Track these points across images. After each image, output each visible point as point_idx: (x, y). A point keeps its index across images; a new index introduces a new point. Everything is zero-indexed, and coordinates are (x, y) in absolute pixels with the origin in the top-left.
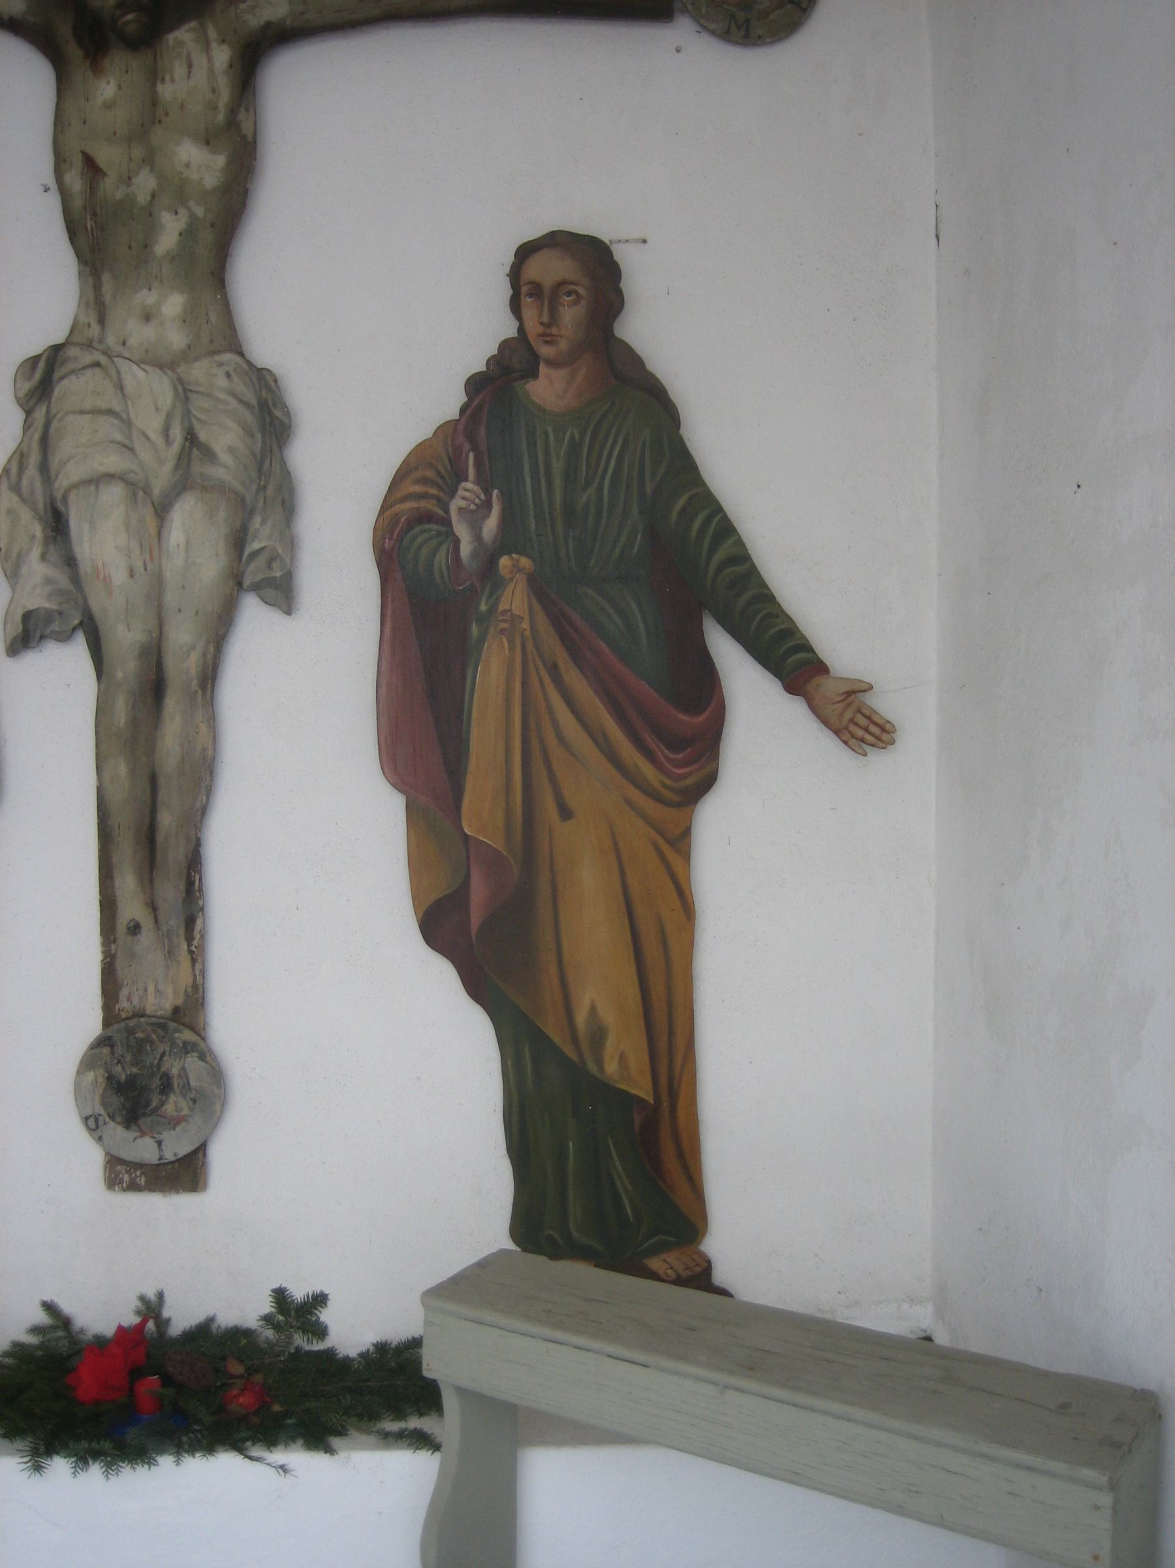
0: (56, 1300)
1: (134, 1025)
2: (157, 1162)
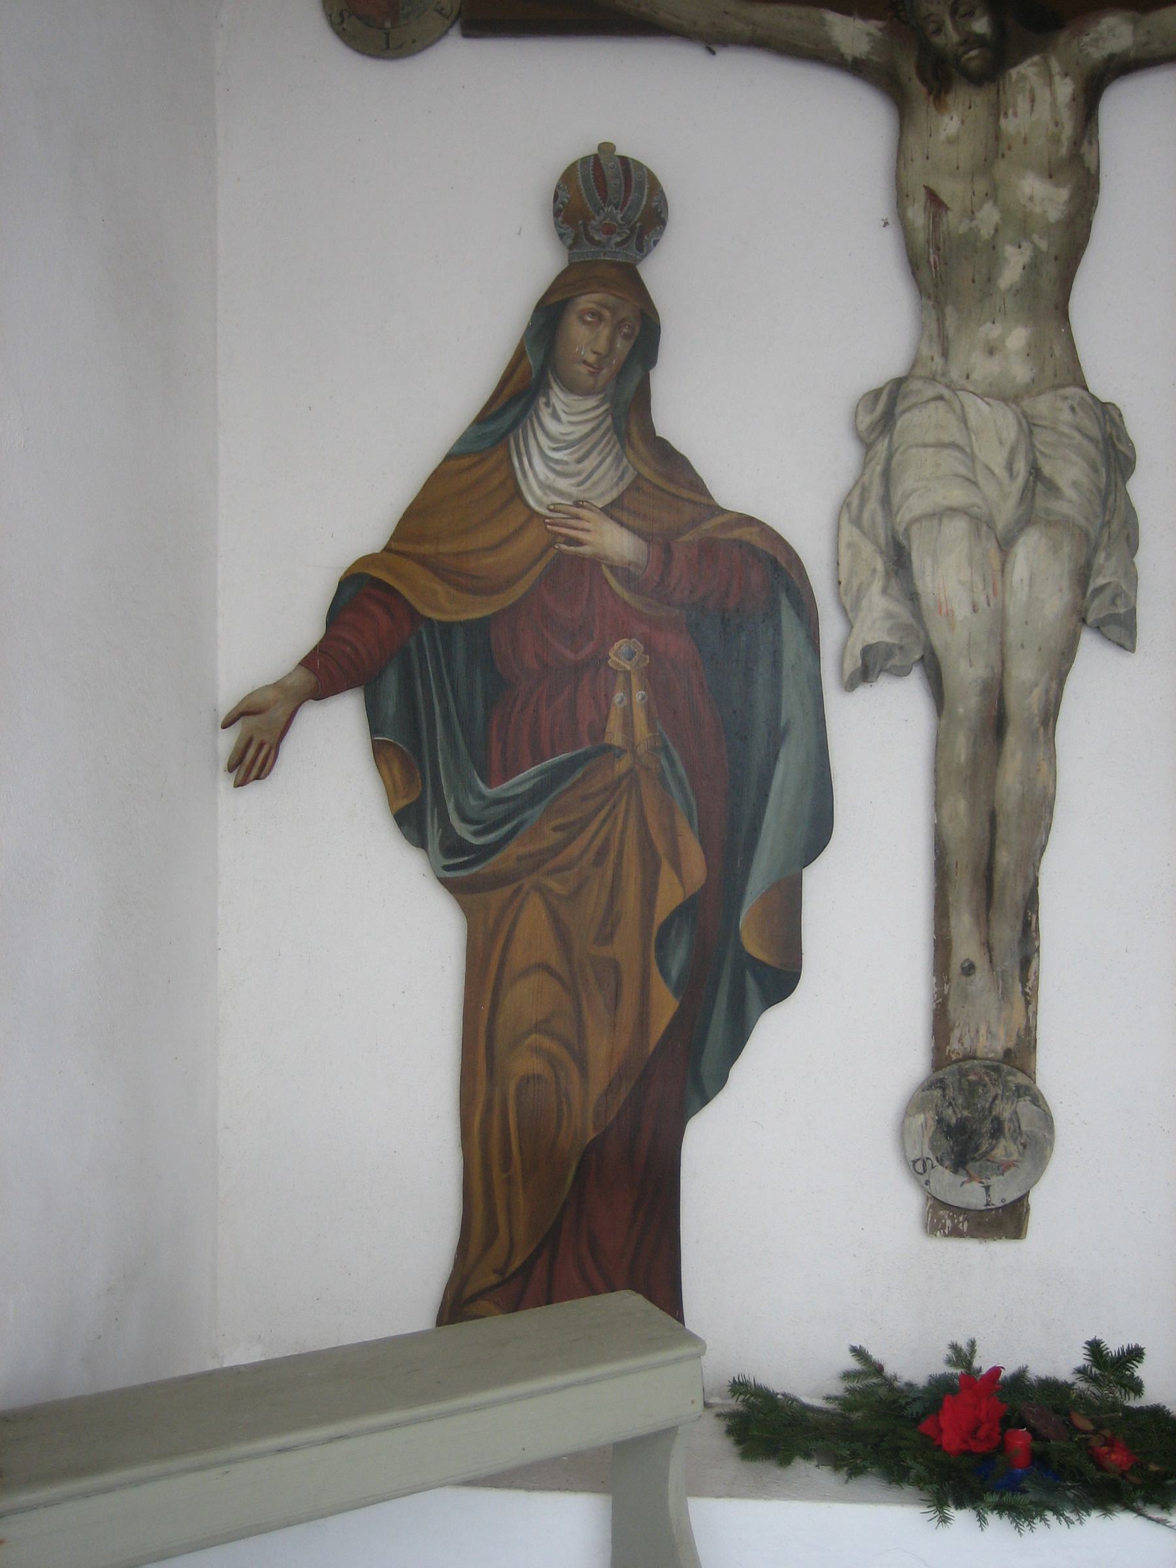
0: (864, 1346)
1: (968, 1068)
2: (984, 1208)
